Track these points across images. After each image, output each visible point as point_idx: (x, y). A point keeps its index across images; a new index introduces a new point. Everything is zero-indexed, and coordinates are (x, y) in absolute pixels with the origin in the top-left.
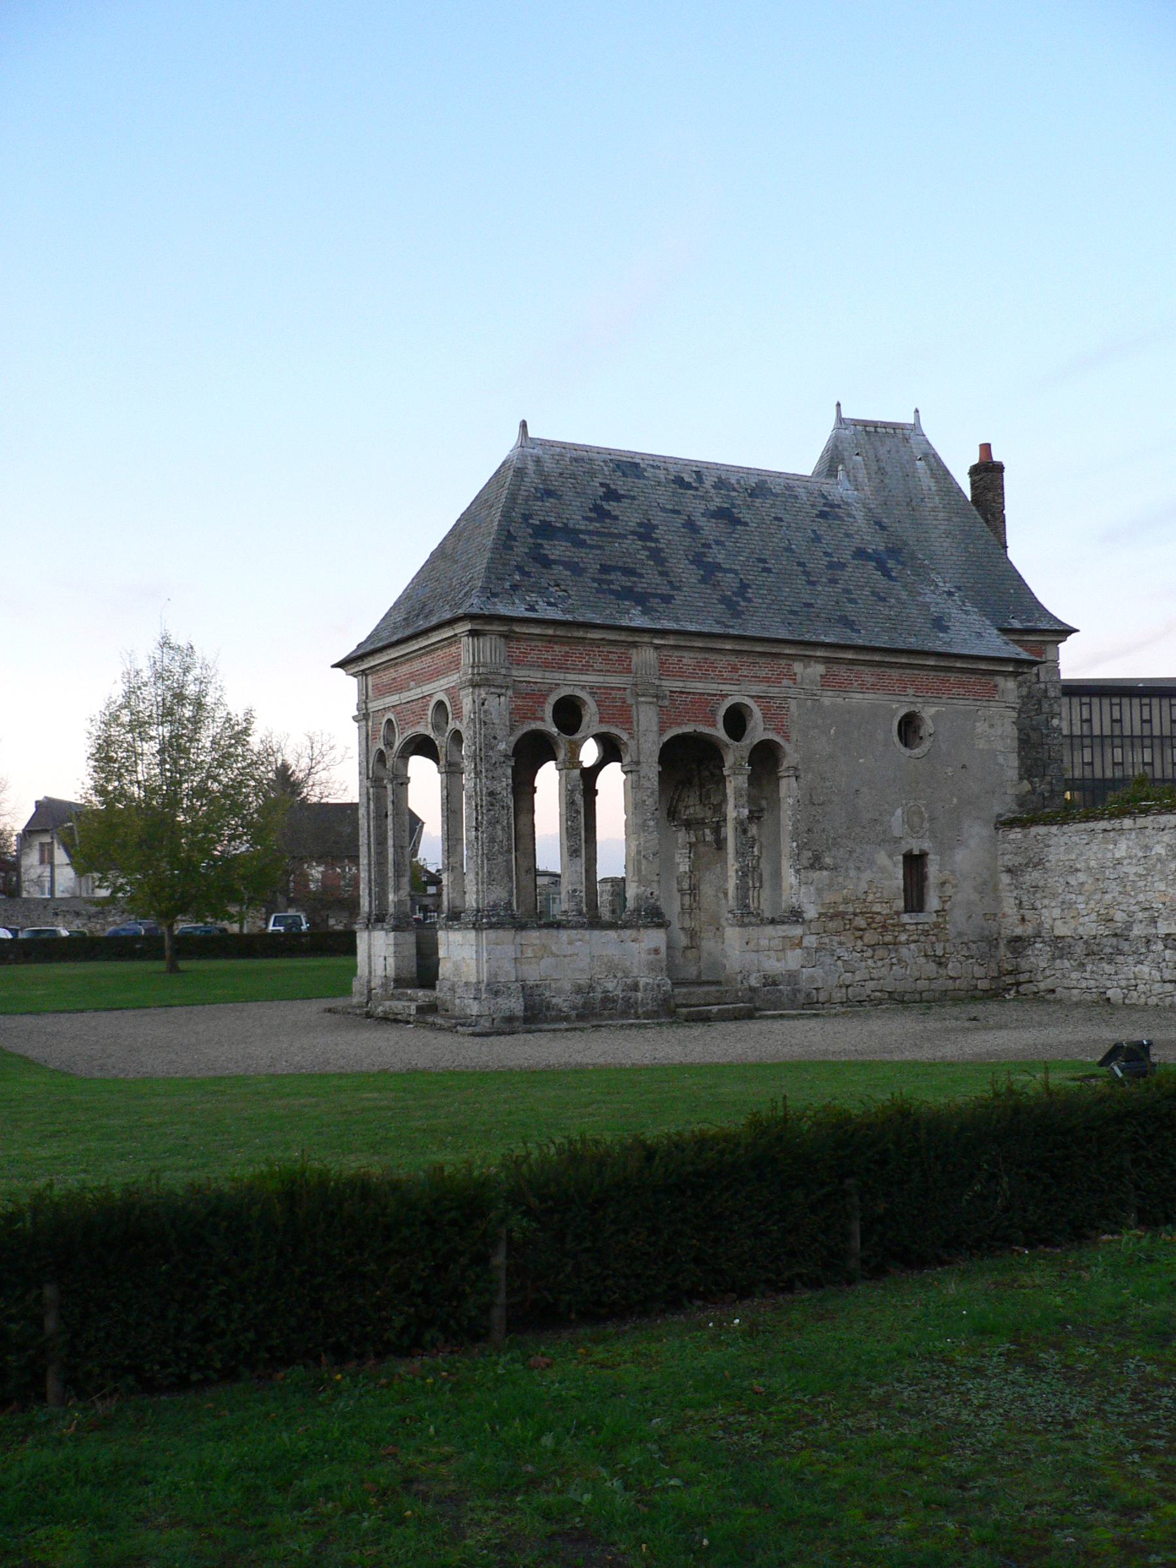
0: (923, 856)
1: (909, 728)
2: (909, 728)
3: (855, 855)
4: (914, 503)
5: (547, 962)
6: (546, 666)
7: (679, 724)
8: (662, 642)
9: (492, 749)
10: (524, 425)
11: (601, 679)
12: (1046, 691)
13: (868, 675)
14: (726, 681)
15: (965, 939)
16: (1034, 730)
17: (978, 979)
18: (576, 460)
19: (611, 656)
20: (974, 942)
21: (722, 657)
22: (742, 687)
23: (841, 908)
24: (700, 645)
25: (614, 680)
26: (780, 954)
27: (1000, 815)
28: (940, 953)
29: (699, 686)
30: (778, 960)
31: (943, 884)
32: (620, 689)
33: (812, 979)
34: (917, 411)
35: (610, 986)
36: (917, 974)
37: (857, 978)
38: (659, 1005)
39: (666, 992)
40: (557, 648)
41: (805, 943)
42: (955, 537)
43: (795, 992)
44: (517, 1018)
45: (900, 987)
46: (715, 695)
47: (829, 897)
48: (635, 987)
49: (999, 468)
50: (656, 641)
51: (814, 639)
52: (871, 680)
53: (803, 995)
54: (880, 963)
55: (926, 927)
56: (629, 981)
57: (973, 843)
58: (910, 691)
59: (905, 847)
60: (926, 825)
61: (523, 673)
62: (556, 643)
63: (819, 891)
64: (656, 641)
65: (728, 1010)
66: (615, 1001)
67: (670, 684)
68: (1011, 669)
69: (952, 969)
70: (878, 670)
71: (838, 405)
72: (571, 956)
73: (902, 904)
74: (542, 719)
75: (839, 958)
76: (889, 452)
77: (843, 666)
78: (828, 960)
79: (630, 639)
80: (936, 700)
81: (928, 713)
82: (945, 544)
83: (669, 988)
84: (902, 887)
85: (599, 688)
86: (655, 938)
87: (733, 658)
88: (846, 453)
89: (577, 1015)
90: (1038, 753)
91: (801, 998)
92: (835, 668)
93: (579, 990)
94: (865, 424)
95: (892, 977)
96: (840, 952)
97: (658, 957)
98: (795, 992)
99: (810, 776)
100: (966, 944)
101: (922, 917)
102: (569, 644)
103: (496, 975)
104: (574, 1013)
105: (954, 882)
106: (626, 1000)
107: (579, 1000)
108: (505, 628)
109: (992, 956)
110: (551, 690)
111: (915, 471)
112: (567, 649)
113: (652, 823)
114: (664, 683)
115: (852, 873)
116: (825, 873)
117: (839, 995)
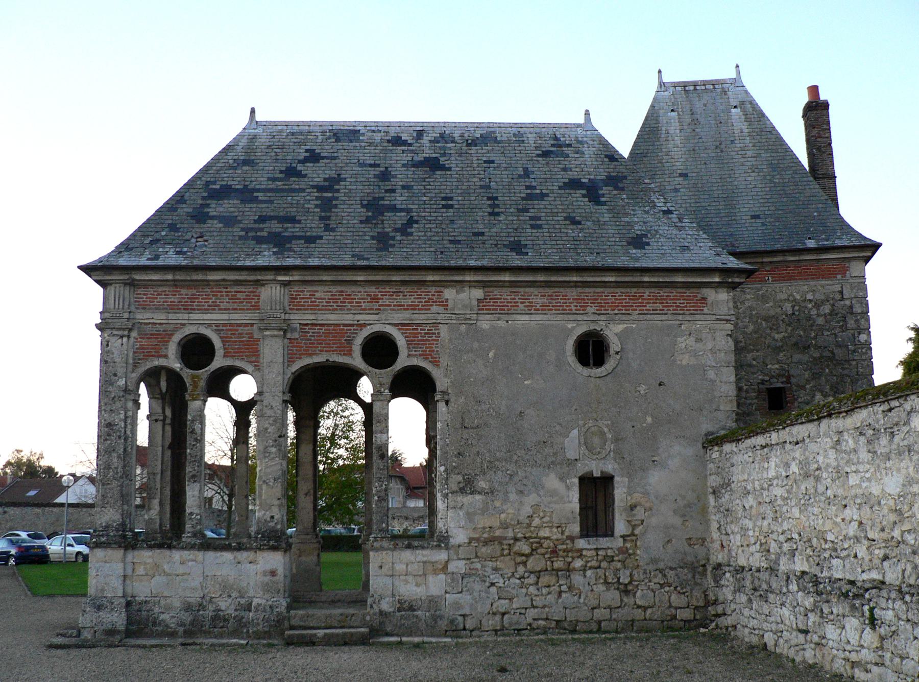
0: (607, 481)
1: (591, 350)
2: (591, 350)
3: (516, 479)
4: (723, 146)
5: (159, 580)
6: (173, 308)
7: (311, 355)
8: (287, 278)
9: (112, 384)
10: (253, 111)
11: (225, 317)
12: (851, 307)
13: (537, 297)
14: (363, 311)
15: (661, 565)
16: (840, 346)
17: (676, 608)
18: (293, 134)
19: (239, 295)
20: (671, 569)
21: (361, 289)
22: (383, 317)
23: (498, 533)
24: (329, 278)
25: (237, 317)
26: (419, 579)
27: (711, 433)
28: (625, 579)
29: (333, 318)
30: (417, 585)
31: (633, 507)
32: (246, 325)
33: (457, 605)
34: (737, 66)
35: (223, 605)
36: (594, 603)
37: (514, 606)
38: (271, 626)
39: (279, 614)
40: (184, 291)
41: (452, 567)
42: (761, 171)
43: (436, 618)
44: (119, 632)
45: (571, 616)
46: (352, 325)
47: (483, 522)
48: (248, 608)
49: (825, 106)
50: (280, 278)
51: (460, 263)
52: (540, 301)
53: (446, 622)
54: (545, 591)
55: (610, 553)
56: (243, 601)
57: (674, 463)
58: (591, 310)
59: (582, 469)
60: (610, 446)
61: (146, 316)
62: (183, 287)
63: (470, 516)
64: (280, 278)
65: (338, 635)
66: (226, 620)
67: (297, 318)
68: (717, 280)
69: (641, 596)
70: (550, 291)
71: (660, 72)
72: (183, 574)
73: (578, 529)
74: (166, 356)
75: (493, 584)
76: (705, 105)
77: (505, 290)
78: (477, 587)
79: (252, 278)
80: (624, 317)
81: (613, 332)
82: (750, 179)
83: (283, 609)
84: (578, 510)
85: (225, 325)
86: (275, 560)
87: (373, 289)
88: (661, 111)
89: (185, 632)
90: (843, 369)
91: (443, 624)
92: (496, 291)
93: (188, 608)
94: (684, 85)
95: (554, 603)
96: (495, 578)
97: (275, 579)
98: (436, 618)
99: (462, 400)
100: (661, 571)
101: (604, 542)
102: (195, 287)
103: (103, 590)
104: (181, 629)
105: (648, 505)
106: (239, 620)
107: (187, 618)
108: (126, 277)
109: (696, 584)
110: (176, 330)
111: (729, 117)
112: (194, 291)
113: (274, 450)
114: (292, 317)
115: (513, 496)
116: (478, 497)
117: (491, 623)
